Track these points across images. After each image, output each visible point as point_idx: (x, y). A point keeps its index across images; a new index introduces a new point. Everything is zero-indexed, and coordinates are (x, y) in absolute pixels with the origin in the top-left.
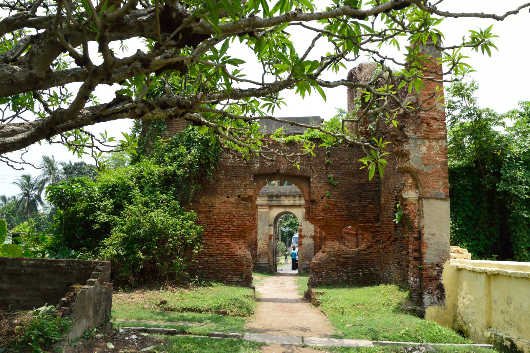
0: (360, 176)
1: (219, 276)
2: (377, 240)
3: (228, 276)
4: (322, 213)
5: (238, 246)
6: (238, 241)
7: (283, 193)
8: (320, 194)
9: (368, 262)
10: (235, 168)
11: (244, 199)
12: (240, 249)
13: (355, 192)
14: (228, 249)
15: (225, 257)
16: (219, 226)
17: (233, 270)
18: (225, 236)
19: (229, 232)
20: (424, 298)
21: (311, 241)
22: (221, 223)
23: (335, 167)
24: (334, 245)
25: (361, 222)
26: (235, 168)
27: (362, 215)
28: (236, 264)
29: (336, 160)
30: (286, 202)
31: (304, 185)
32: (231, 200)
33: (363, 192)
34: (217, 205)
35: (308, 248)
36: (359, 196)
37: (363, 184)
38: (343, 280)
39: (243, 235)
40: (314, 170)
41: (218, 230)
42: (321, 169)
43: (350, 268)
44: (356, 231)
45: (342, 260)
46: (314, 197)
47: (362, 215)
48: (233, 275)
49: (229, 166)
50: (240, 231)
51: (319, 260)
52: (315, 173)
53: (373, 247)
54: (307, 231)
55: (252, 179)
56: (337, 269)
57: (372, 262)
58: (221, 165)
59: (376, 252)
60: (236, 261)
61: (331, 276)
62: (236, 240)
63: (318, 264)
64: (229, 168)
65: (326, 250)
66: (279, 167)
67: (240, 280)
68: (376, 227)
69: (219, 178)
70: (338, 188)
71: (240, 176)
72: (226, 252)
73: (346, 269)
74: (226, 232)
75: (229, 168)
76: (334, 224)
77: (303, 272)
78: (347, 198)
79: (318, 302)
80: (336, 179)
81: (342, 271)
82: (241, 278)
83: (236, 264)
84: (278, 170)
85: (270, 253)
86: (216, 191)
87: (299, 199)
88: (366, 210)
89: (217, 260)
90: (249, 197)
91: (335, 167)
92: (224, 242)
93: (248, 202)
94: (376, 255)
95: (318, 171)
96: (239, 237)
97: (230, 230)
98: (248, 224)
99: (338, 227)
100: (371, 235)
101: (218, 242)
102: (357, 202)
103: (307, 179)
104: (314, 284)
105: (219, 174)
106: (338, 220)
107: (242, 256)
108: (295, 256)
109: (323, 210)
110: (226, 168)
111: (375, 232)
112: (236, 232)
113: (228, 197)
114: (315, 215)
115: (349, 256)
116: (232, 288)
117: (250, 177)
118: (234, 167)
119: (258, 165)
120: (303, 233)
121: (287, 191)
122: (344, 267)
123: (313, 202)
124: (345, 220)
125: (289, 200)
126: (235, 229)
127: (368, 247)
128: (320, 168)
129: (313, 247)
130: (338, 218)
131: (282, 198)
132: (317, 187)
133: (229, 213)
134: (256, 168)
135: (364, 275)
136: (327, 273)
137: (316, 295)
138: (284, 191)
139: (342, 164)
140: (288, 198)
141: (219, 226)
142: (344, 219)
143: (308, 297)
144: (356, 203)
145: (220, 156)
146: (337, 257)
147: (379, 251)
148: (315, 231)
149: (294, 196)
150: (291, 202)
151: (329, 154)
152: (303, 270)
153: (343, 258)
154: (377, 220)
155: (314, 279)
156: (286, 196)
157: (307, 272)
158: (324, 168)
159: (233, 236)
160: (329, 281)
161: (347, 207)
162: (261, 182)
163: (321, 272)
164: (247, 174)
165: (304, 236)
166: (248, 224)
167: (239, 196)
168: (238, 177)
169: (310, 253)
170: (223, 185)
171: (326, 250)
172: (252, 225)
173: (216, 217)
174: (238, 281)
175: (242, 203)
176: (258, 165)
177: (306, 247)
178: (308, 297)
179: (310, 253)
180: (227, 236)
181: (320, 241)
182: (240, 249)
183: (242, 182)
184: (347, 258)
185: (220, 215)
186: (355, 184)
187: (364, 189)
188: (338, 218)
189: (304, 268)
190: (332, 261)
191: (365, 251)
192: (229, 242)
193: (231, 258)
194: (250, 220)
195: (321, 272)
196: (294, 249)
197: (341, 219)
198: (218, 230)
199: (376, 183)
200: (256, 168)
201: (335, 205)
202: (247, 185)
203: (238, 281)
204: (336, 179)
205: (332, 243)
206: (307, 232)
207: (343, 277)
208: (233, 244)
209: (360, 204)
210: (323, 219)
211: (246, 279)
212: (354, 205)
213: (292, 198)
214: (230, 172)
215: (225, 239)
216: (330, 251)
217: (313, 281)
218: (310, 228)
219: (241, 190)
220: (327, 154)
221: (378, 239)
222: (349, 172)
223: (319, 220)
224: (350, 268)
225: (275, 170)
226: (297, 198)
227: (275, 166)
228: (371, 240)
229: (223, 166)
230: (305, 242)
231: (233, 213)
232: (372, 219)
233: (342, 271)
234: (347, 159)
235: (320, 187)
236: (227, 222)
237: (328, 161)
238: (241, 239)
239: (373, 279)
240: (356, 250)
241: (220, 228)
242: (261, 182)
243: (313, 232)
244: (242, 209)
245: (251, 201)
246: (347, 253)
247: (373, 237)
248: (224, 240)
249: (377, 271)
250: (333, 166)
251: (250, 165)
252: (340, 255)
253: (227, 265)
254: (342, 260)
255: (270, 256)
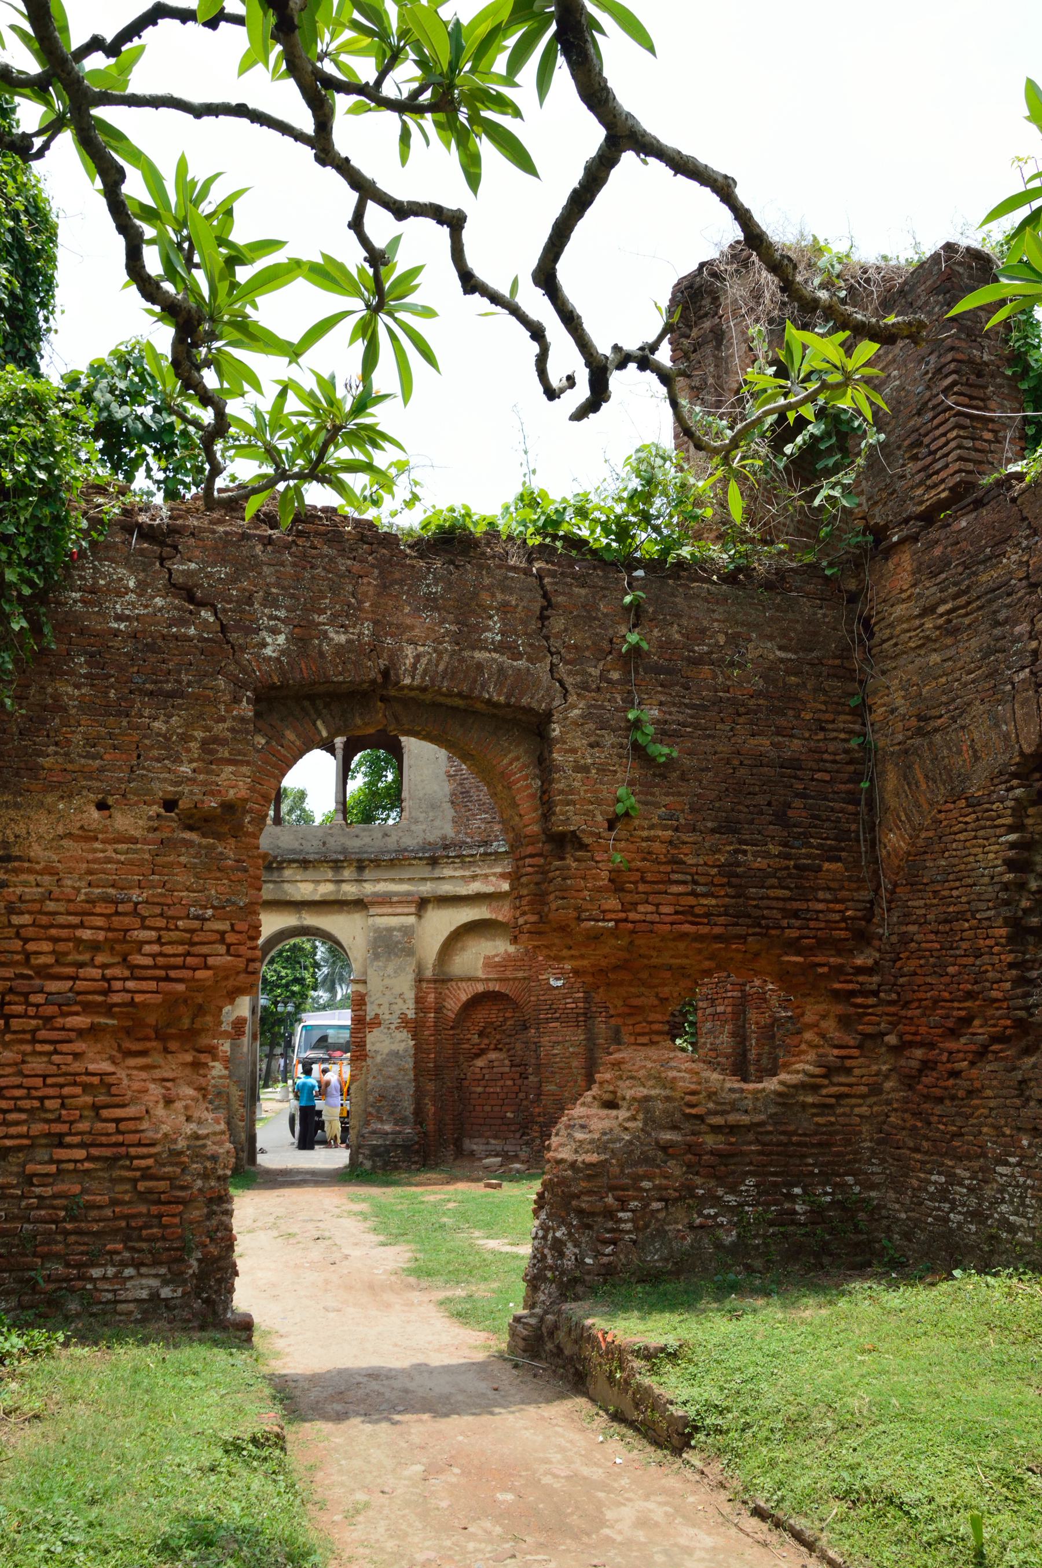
0: (782, 722)
1: (39, 1275)
2: (867, 1036)
3: (96, 1273)
4: (612, 903)
5: (156, 1090)
6: (156, 1058)
7: (294, 851)
8: (599, 802)
9: (827, 1144)
10: (151, 648)
11: (199, 821)
12: (168, 1102)
13: (761, 800)
14: (96, 1108)
15: (81, 1154)
16: (44, 973)
17: (127, 1236)
18: (81, 1033)
19: (108, 1010)
20: (951, 1277)
21: (402, 1042)
22: (60, 958)
23: (668, 672)
24: (665, 1063)
25: (793, 946)
26: (151, 648)
27: (795, 914)
28: (142, 1197)
29: (670, 641)
30: (305, 889)
31: (514, 761)
32: (123, 821)
33: (797, 803)
34: (36, 851)
35: (391, 1070)
36: (781, 818)
37: (794, 764)
38: (719, 1245)
39: (186, 1023)
40: (569, 681)
41: (39, 999)
42: (603, 677)
43: (750, 1181)
44: (586, 1000)
45: (710, 1141)
46: (570, 818)
47: (795, 914)
48: (124, 1264)
49: (116, 633)
50: (172, 1002)
51: (600, 1146)
52: (572, 699)
53: (848, 1071)
54: (384, 1001)
55: (246, 709)
56: (690, 1189)
57: (848, 1142)
58: (66, 624)
59: (863, 1096)
60: (147, 1175)
61: (661, 1233)
62: (143, 1053)
63: (593, 1171)
64: (117, 643)
65: (629, 1091)
66: (395, 657)
67: (166, 1292)
68: (860, 970)
69: (56, 697)
70: (683, 778)
71: (182, 695)
72: (83, 1126)
73: (733, 1190)
74: (88, 1008)
75: (117, 643)
76: (34, 1022)
77: (368, 1164)
78: (728, 827)
79: (685, 1421)
80: (675, 734)
81: (716, 1201)
82: (174, 1279)
83: (142, 1197)
84: (386, 673)
85: (235, 1093)
86: (34, 770)
87: (355, 876)
88: (815, 889)
89: (29, 1179)
90: (229, 807)
91: (668, 672)
92: (77, 1067)
93: (219, 837)
94: (864, 1110)
95: (587, 688)
96: (161, 1036)
97: (116, 998)
98: (221, 959)
99: (681, 972)
100: (839, 1009)
101: (36, 1065)
102: (775, 850)
103: (534, 728)
104: (575, 1281)
105: (55, 673)
106: (684, 936)
107: (181, 1144)
108: (311, 1098)
109: (616, 884)
110: (100, 650)
111: (852, 993)
112: (144, 1005)
113: (102, 806)
114: (579, 909)
115: (745, 1119)
116: (128, 1355)
117: (237, 700)
118: (147, 643)
119: (281, 639)
120: (371, 1011)
121: (307, 847)
122: (721, 1180)
123: (563, 842)
124: (718, 938)
125: (317, 882)
126: (146, 992)
127: (830, 1071)
128: (595, 672)
129: (409, 1064)
130: (687, 928)
131: (287, 873)
132: (585, 769)
133: (107, 899)
134: (268, 651)
135: (817, 1213)
136: (643, 1215)
137: (638, 1364)
138: (296, 845)
139: (697, 662)
140: (310, 874)
141: (44, 973)
142: (717, 930)
143: (550, 1356)
144: (767, 855)
145: (68, 576)
146: (687, 1126)
147: (875, 1090)
148: (419, 1000)
149: (337, 865)
150: (325, 890)
151: (636, 608)
152: (370, 1157)
153: (716, 1129)
154: (863, 938)
155: (570, 1250)
156: (305, 864)
157: (386, 1163)
158: (615, 675)
159: (128, 1032)
160: (654, 1258)
161: (729, 871)
162: (290, 735)
163: (609, 1214)
164: (221, 682)
165: (376, 1022)
166: (221, 959)
167: (170, 805)
168: (167, 698)
169: (398, 1088)
170: (77, 738)
171: (629, 1091)
172: (241, 963)
173: (26, 919)
174: (155, 1296)
175: (188, 844)
176: (281, 639)
177: (384, 1063)
178: (550, 1356)
179: (398, 1088)
180: (92, 1032)
181: (437, 1042)
182: (168, 1102)
183: (188, 725)
184: (733, 1129)
185: (51, 906)
186: (759, 760)
187: (799, 786)
188: (687, 928)
189: (374, 1148)
190: (665, 1148)
191: (815, 1088)
192: (106, 1066)
193: (116, 1159)
194: (231, 938)
195: (609, 1214)
196: (308, 1072)
197: (704, 930)
198: (39, 999)
199: (851, 762)
200: (268, 651)
201: (675, 861)
202: (215, 740)
203: (155, 1296)
204: (675, 734)
205: (653, 1052)
206: (385, 1009)
207: (720, 1233)
208: (128, 1077)
209: (787, 857)
210: (614, 933)
211: (202, 1276)
212: (760, 863)
213: (330, 875)
214: (122, 669)
215: (79, 1046)
216: (647, 1099)
217: (569, 1263)
218: (397, 990)
219: (185, 769)
220: (628, 608)
221: (870, 1029)
222: (733, 702)
223: (595, 937)
224: (750, 1181)
225: (372, 670)
226: (347, 874)
227: (375, 649)
228: (835, 1034)
229: (81, 632)
230: (378, 1047)
231: (135, 895)
232: (843, 934)
233: (716, 1201)
234: (722, 639)
235: (602, 770)
236: (95, 947)
237: (633, 638)
238: (173, 1045)
239: (857, 1231)
240: (771, 1084)
241: (53, 986)
242: (290, 735)
243: (411, 1004)
244: (182, 878)
245: (237, 832)
246: (734, 1107)
247: (845, 1022)
248: (77, 1056)
249: (873, 1187)
250: (657, 670)
251: (233, 636)
252: (700, 1118)
253: (91, 1206)
254: (710, 1141)
255: (236, 1104)
